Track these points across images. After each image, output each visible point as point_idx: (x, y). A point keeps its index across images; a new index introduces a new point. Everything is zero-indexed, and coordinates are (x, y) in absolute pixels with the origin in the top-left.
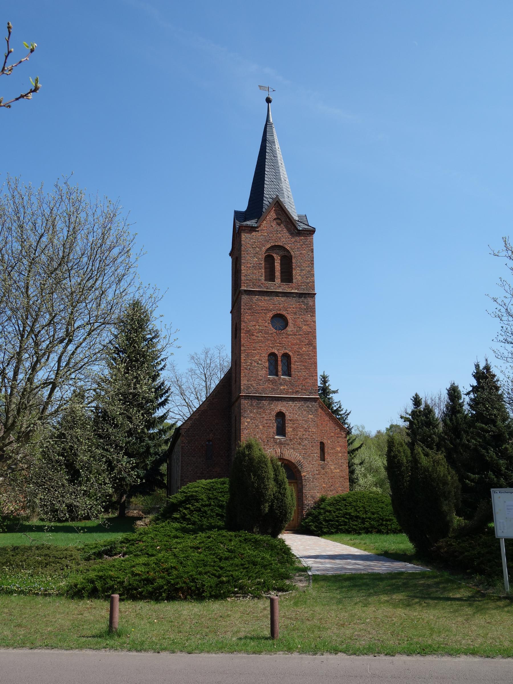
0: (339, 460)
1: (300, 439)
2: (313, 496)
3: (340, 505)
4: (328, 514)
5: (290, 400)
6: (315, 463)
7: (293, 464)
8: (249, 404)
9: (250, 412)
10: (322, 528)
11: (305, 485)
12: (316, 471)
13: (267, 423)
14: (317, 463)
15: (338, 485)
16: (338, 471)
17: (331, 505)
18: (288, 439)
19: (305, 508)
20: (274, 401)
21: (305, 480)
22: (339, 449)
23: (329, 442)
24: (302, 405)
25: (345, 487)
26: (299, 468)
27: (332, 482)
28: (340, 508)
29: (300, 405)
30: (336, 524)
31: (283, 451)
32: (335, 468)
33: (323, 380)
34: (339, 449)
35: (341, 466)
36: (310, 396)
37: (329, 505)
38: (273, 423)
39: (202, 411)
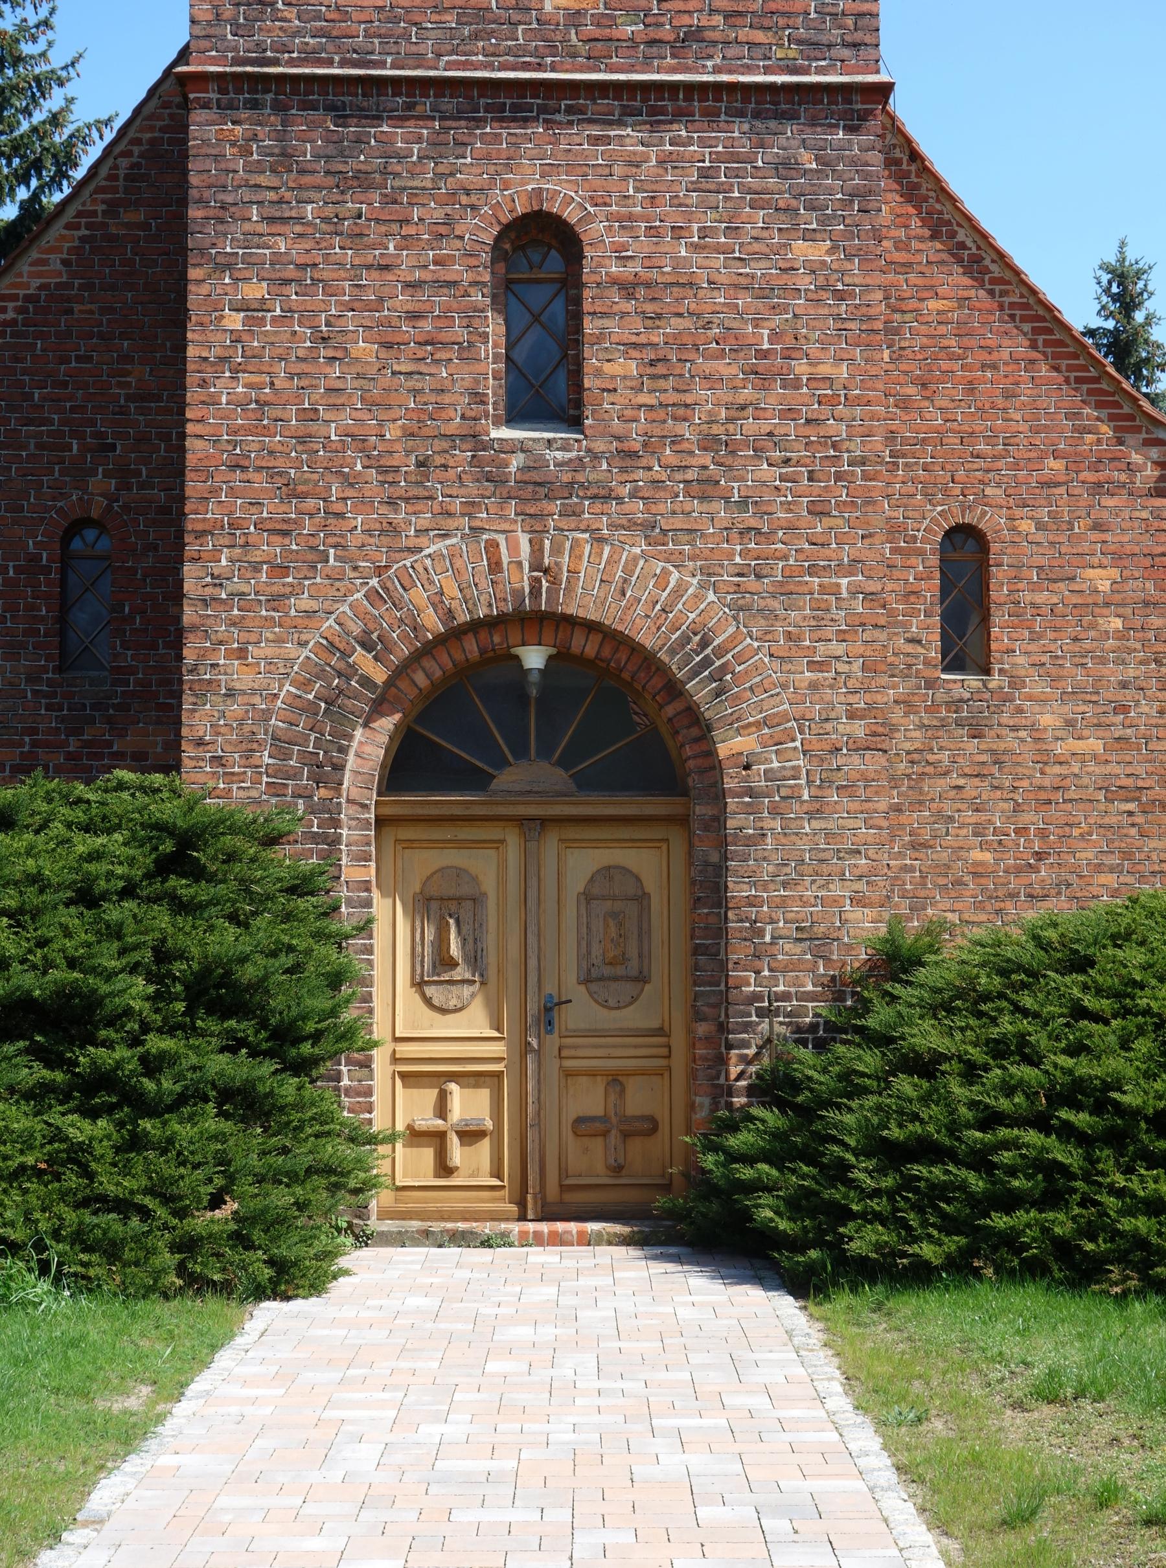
0: (1103, 661)
1: (709, 443)
2: (820, 930)
3: (1025, 1013)
4: (905, 1085)
5: (628, 112)
6: (838, 649)
7: (647, 659)
8: (263, 152)
9: (271, 220)
10: (846, 1215)
11: (750, 841)
12: (852, 715)
13: (414, 316)
14: (858, 648)
15: (1087, 855)
16: (1094, 744)
17: (950, 1011)
18: (599, 446)
19: (747, 1027)
20: (480, 122)
21: (750, 793)
22: (1102, 580)
23: (1027, 526)
24: (735, 158)
25: (1147, 867)
26: (699, 691)
27: (1043, 834)
28: (1022, 1037)
29: (718, 158)
30: (963, 1187)
31: (557, 550)
32: (1070, 723)
33: (1115, 289)
34: (1102, 580)
35: (1122, 709)
36: (806, 71)
37: (933, 1010)
38: (471, 315)
39: (28, 298)
